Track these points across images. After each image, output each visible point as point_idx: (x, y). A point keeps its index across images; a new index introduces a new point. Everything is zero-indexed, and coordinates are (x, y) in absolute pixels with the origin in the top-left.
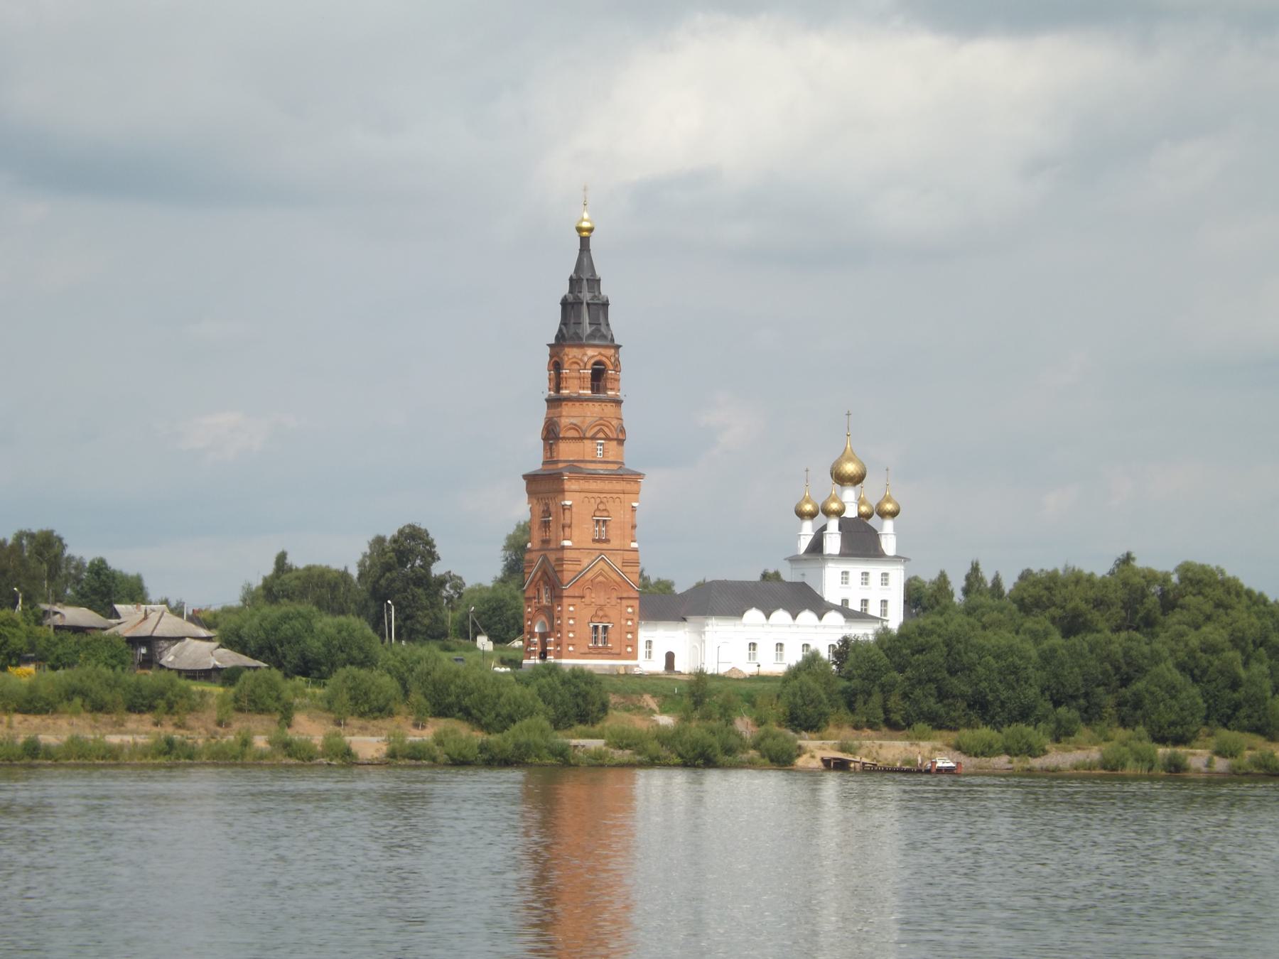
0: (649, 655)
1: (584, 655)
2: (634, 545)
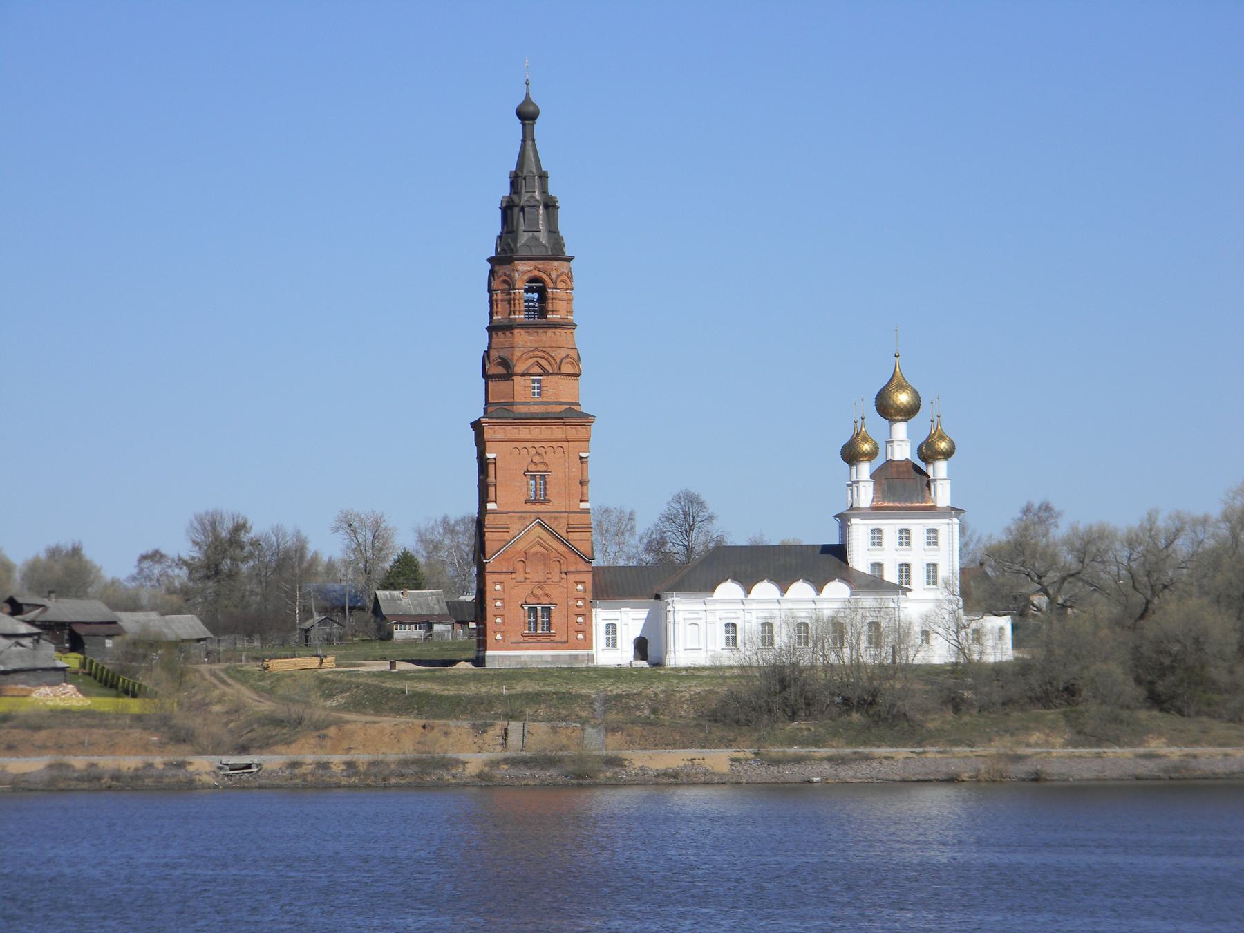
0: (612, 643)
1: (516, 645)
2: (583, 505)
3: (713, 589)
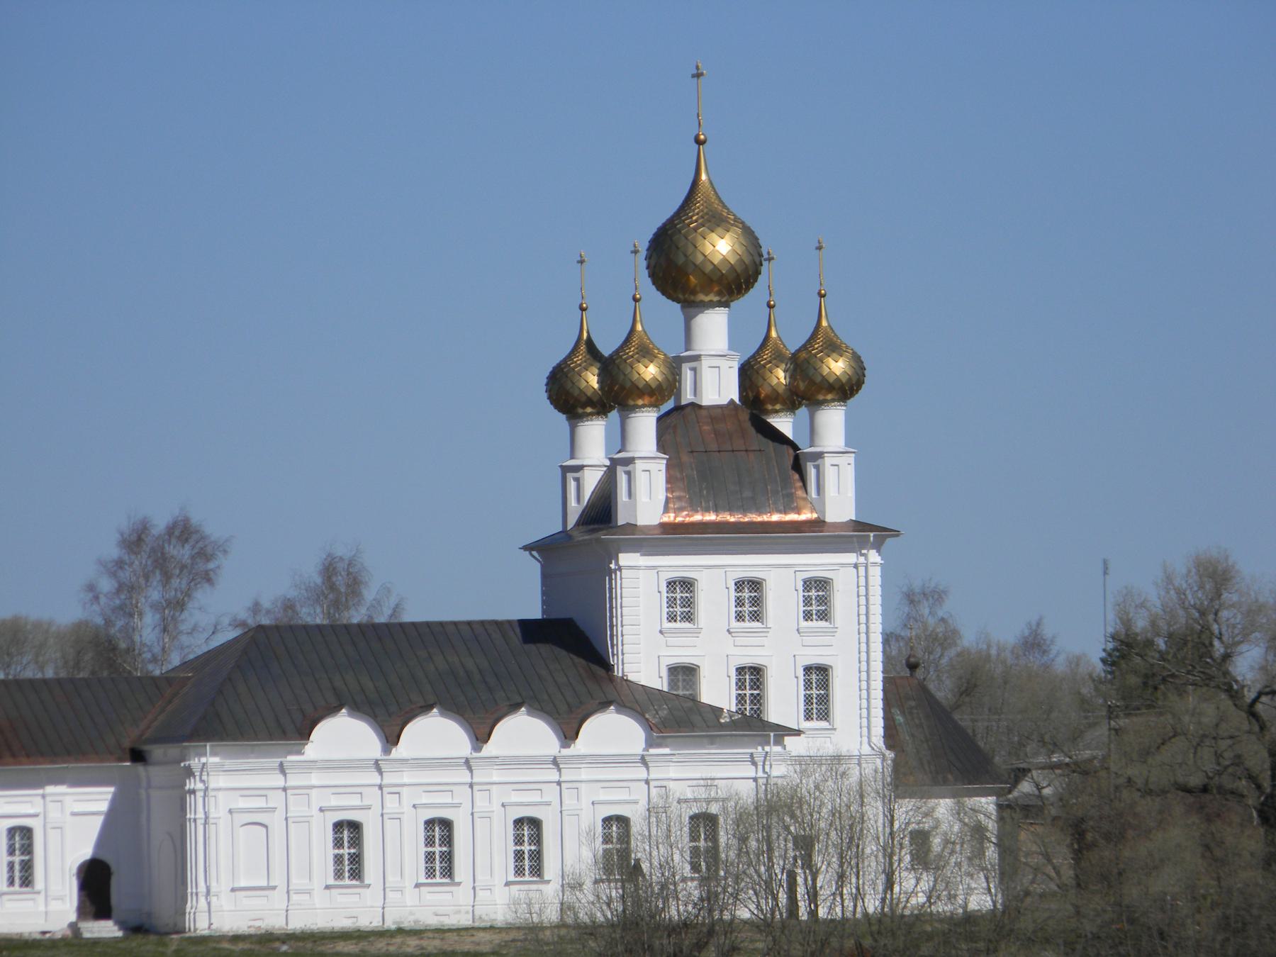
3: (304, 733)
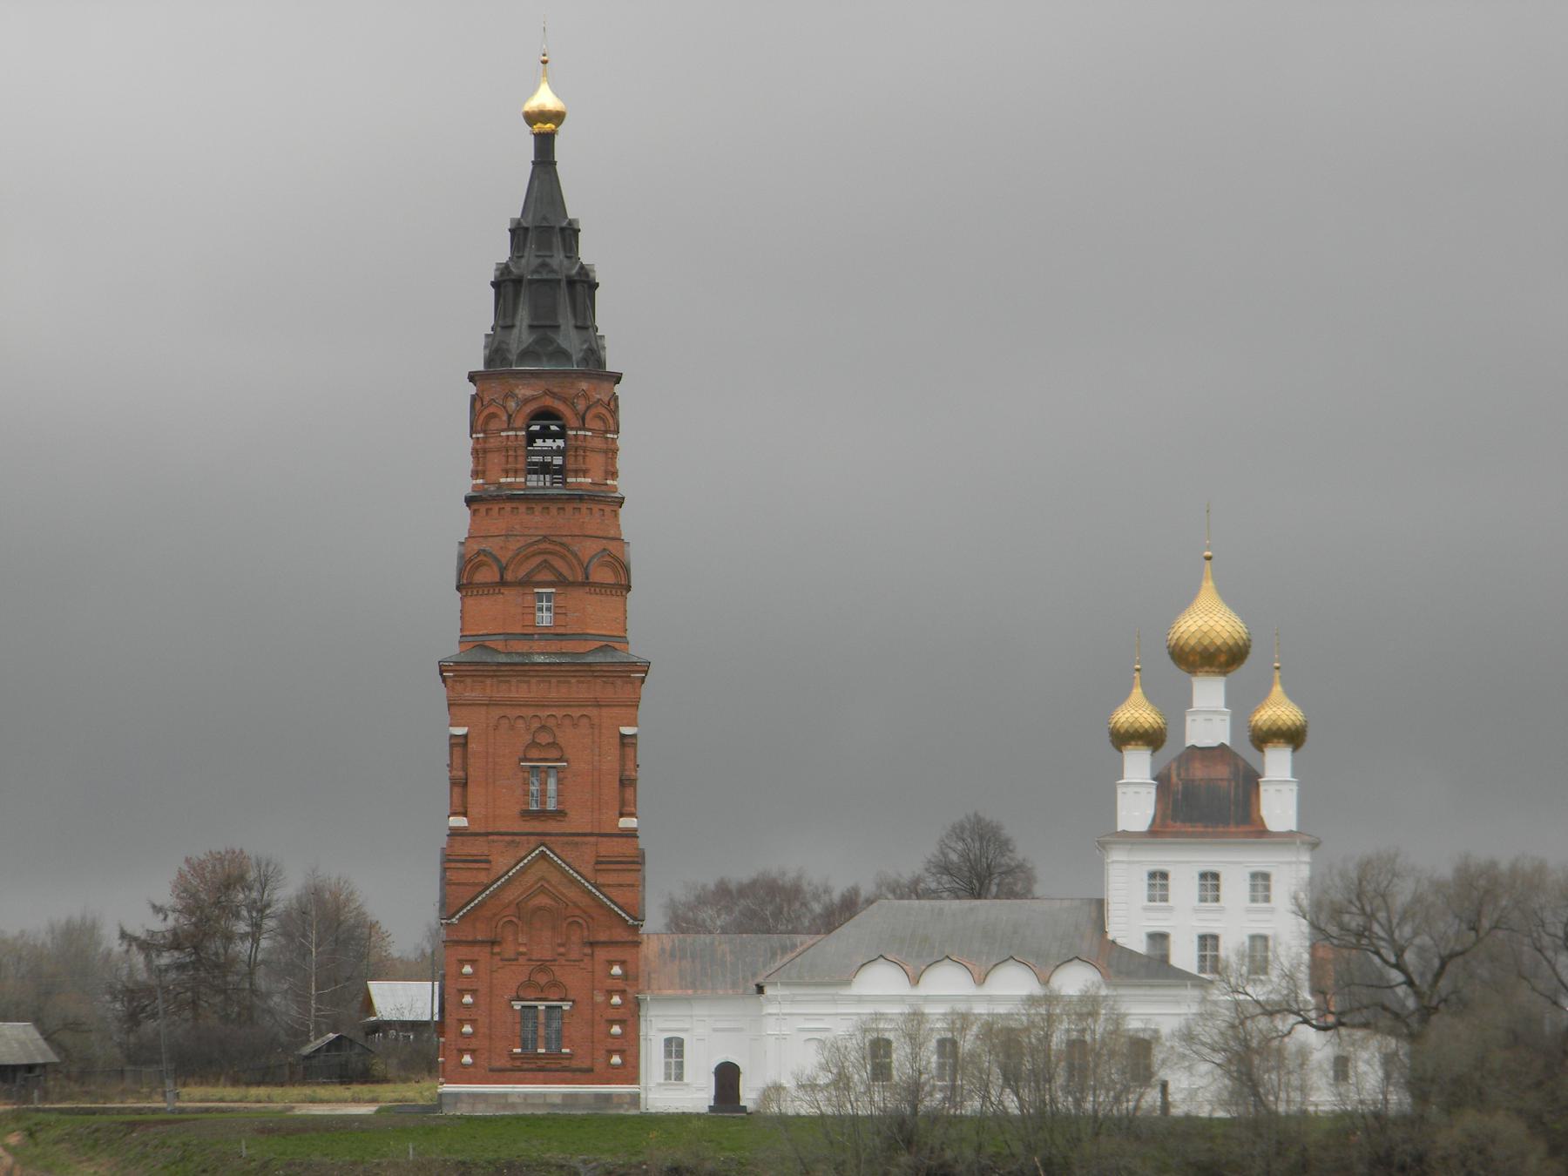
0: (676, 1072)
2: (626, 823)
